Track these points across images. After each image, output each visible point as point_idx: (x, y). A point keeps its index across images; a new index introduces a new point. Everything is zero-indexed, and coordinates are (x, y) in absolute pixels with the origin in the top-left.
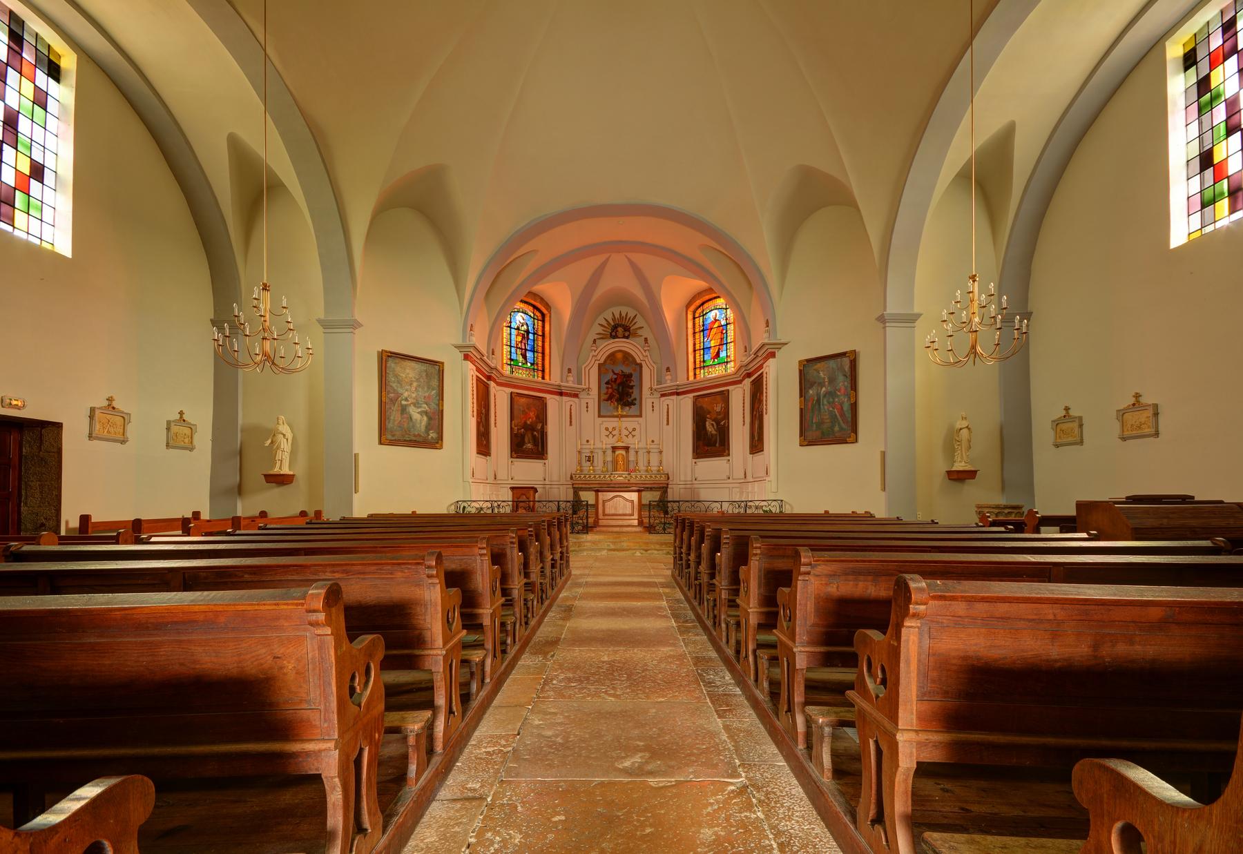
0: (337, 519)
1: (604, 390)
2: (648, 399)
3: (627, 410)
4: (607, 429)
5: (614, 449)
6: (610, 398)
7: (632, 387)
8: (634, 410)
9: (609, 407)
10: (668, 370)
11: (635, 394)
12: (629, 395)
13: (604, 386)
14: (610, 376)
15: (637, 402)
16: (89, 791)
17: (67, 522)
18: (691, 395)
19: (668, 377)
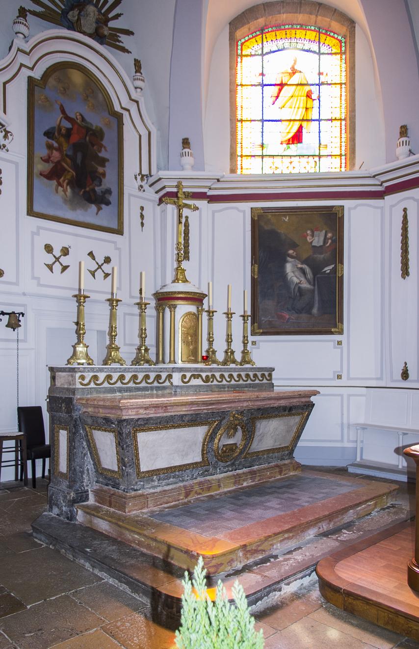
0: (386, 197)
1: (41, 151)
2: (135, 197)
3: (90, 214)
4: (49, 249)
5: (164, 299)
6: (55, 174)
7: (103, 162)
8: (105, 216)
9: (53, 196)
10: (186, 143)
11: (109, 182)
12: (98, 178)
13: (41, 140)
14: (54, 119)
15: (113, 198)
16: (100, 5)
17: (66, 365)
18: (247, 207)
19: (188, 161)
